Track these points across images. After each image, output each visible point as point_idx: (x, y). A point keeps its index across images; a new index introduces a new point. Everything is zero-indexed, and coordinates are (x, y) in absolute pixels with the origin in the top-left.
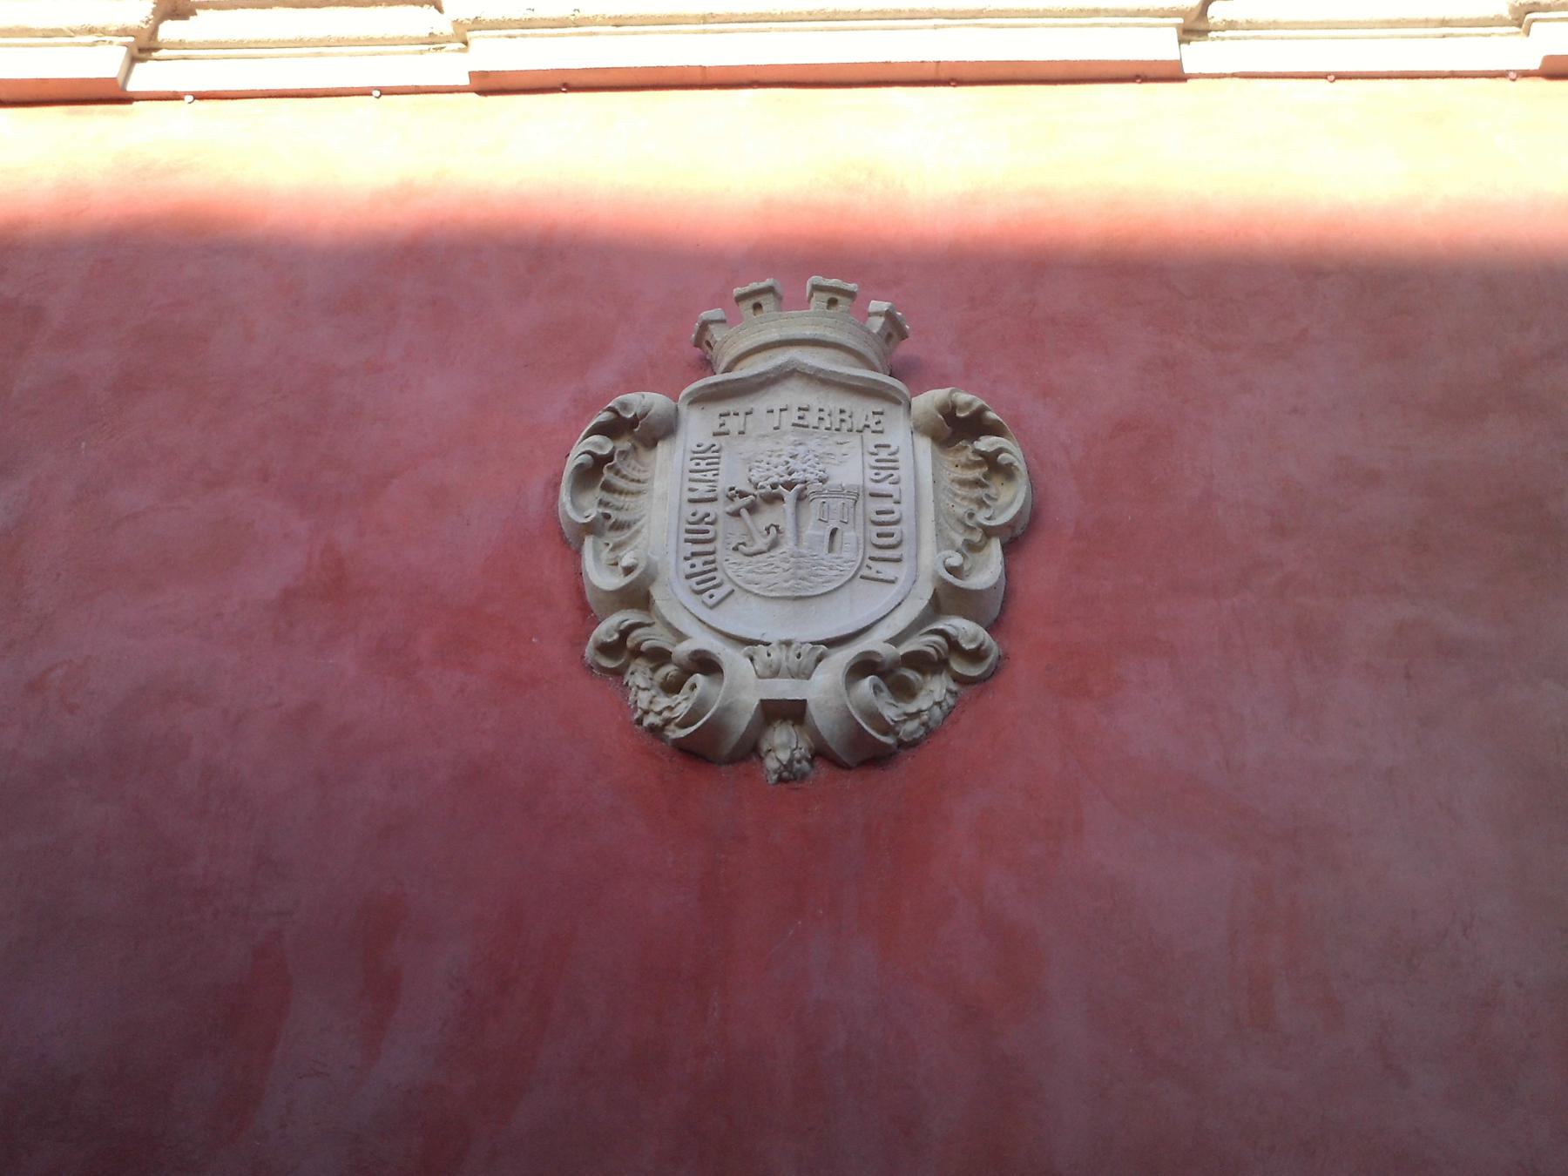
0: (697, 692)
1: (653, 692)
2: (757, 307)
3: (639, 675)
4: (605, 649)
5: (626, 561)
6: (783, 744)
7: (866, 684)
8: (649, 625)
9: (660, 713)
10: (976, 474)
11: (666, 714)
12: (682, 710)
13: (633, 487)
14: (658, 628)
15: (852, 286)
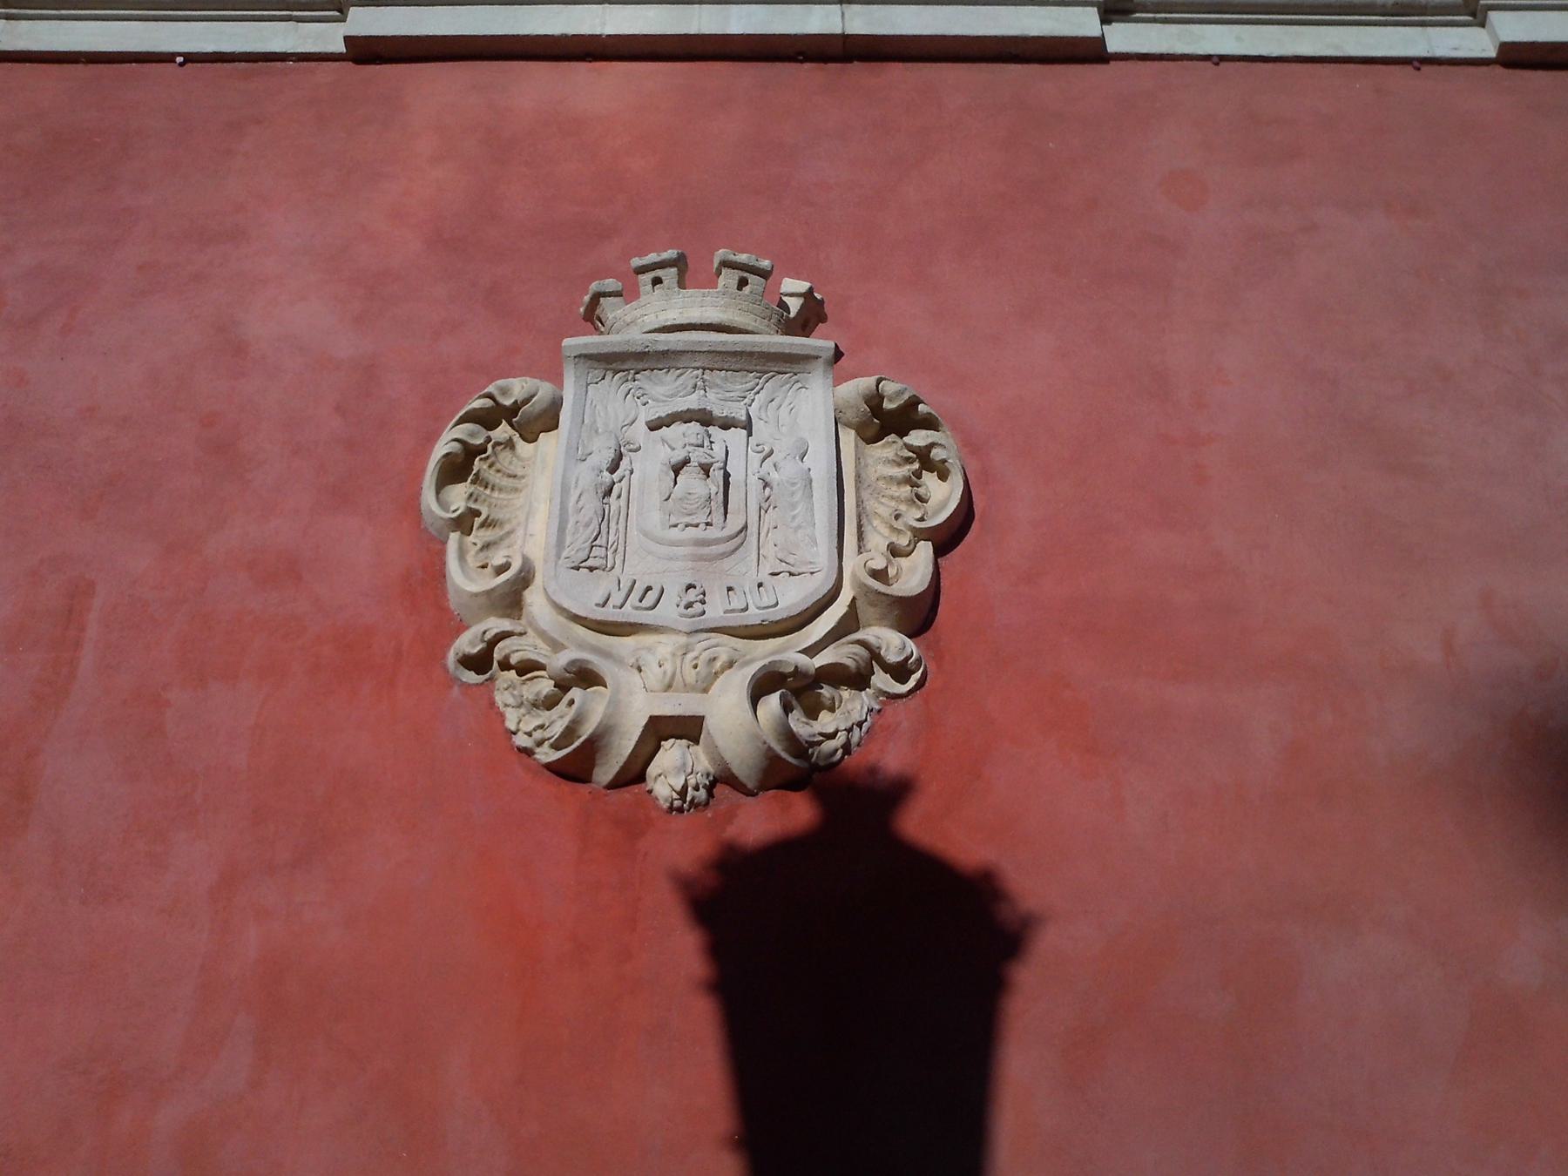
0: (574, 707)
1: (523, 710)
2: (657, 281)
3: (507, 691)
4: (468, 662)
5: (498, 560)
6: (672, 770)
7: (772, 702)
8: (521, 634)
9: (529, 734)
10: (906, 470)
11: (538, 735)
12: (557, 729)
13: (506, 482)
14: (532, 638)
15: (765, 263)
